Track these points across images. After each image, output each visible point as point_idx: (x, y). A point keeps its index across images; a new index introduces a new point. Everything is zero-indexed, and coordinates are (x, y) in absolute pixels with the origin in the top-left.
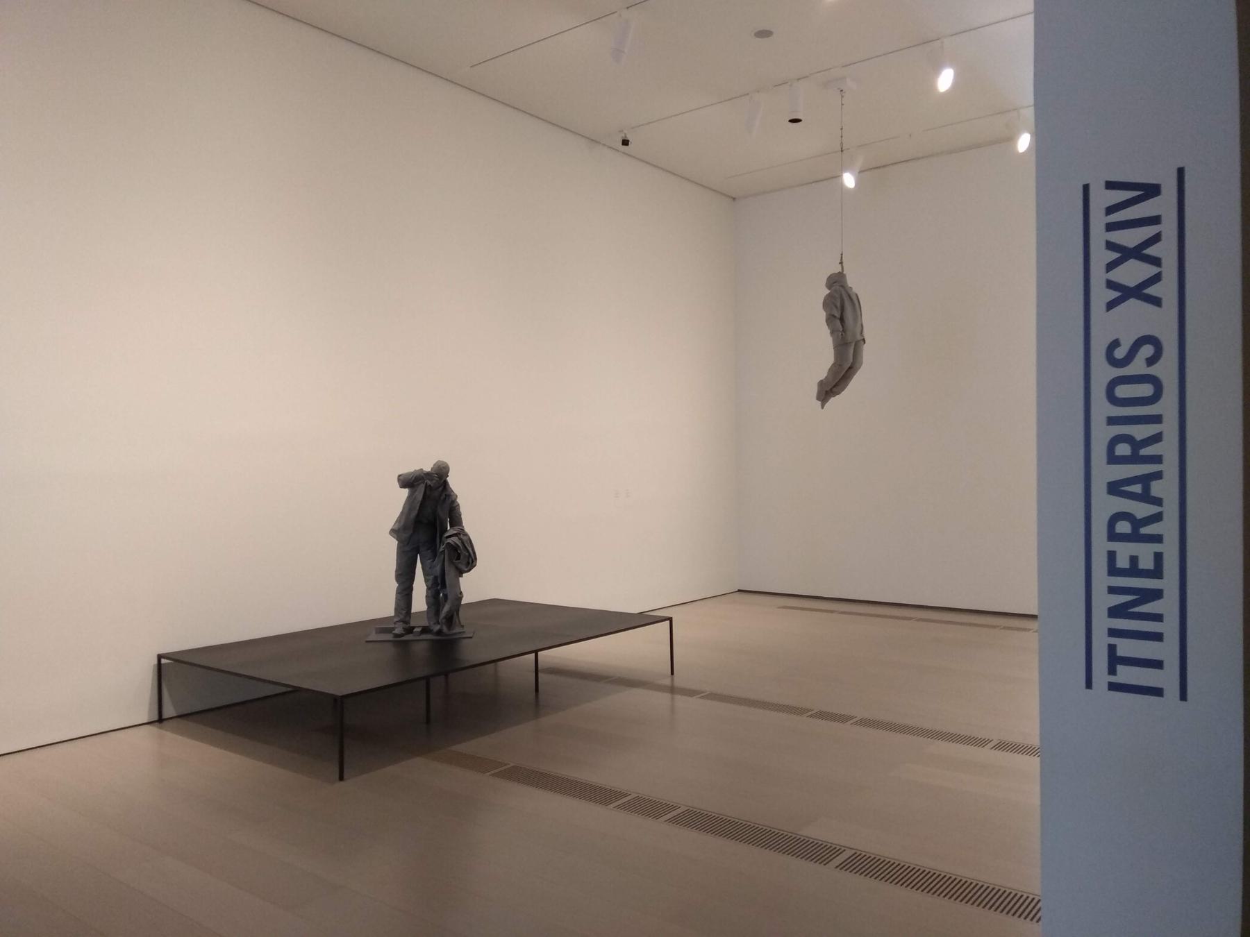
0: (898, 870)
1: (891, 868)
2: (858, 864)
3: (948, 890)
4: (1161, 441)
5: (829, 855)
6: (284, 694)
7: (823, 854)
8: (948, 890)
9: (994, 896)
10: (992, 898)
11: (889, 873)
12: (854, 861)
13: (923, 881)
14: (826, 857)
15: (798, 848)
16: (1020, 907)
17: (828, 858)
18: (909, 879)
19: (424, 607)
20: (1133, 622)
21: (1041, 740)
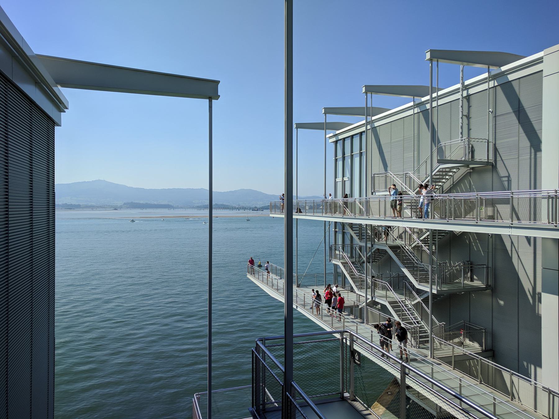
0: (27, 313)
1: (38, 307)
2: (23, 353)
3: (27, 337)
4: (543, 63)
5: (26, 349)
6: (308, 286)
7: (28, 354)
8: (27, 337)
9: (21, 322)
10: (15, 322)
11: (3, 385)
12: (39, 319)
13: (14, 354)
14: (16, 397)
15: (14, 356)
16: (13, 352)
17: (36, 353)
18: (26, 331)
19: (503, 70)
20: (394, 111)
21: (331, 133)
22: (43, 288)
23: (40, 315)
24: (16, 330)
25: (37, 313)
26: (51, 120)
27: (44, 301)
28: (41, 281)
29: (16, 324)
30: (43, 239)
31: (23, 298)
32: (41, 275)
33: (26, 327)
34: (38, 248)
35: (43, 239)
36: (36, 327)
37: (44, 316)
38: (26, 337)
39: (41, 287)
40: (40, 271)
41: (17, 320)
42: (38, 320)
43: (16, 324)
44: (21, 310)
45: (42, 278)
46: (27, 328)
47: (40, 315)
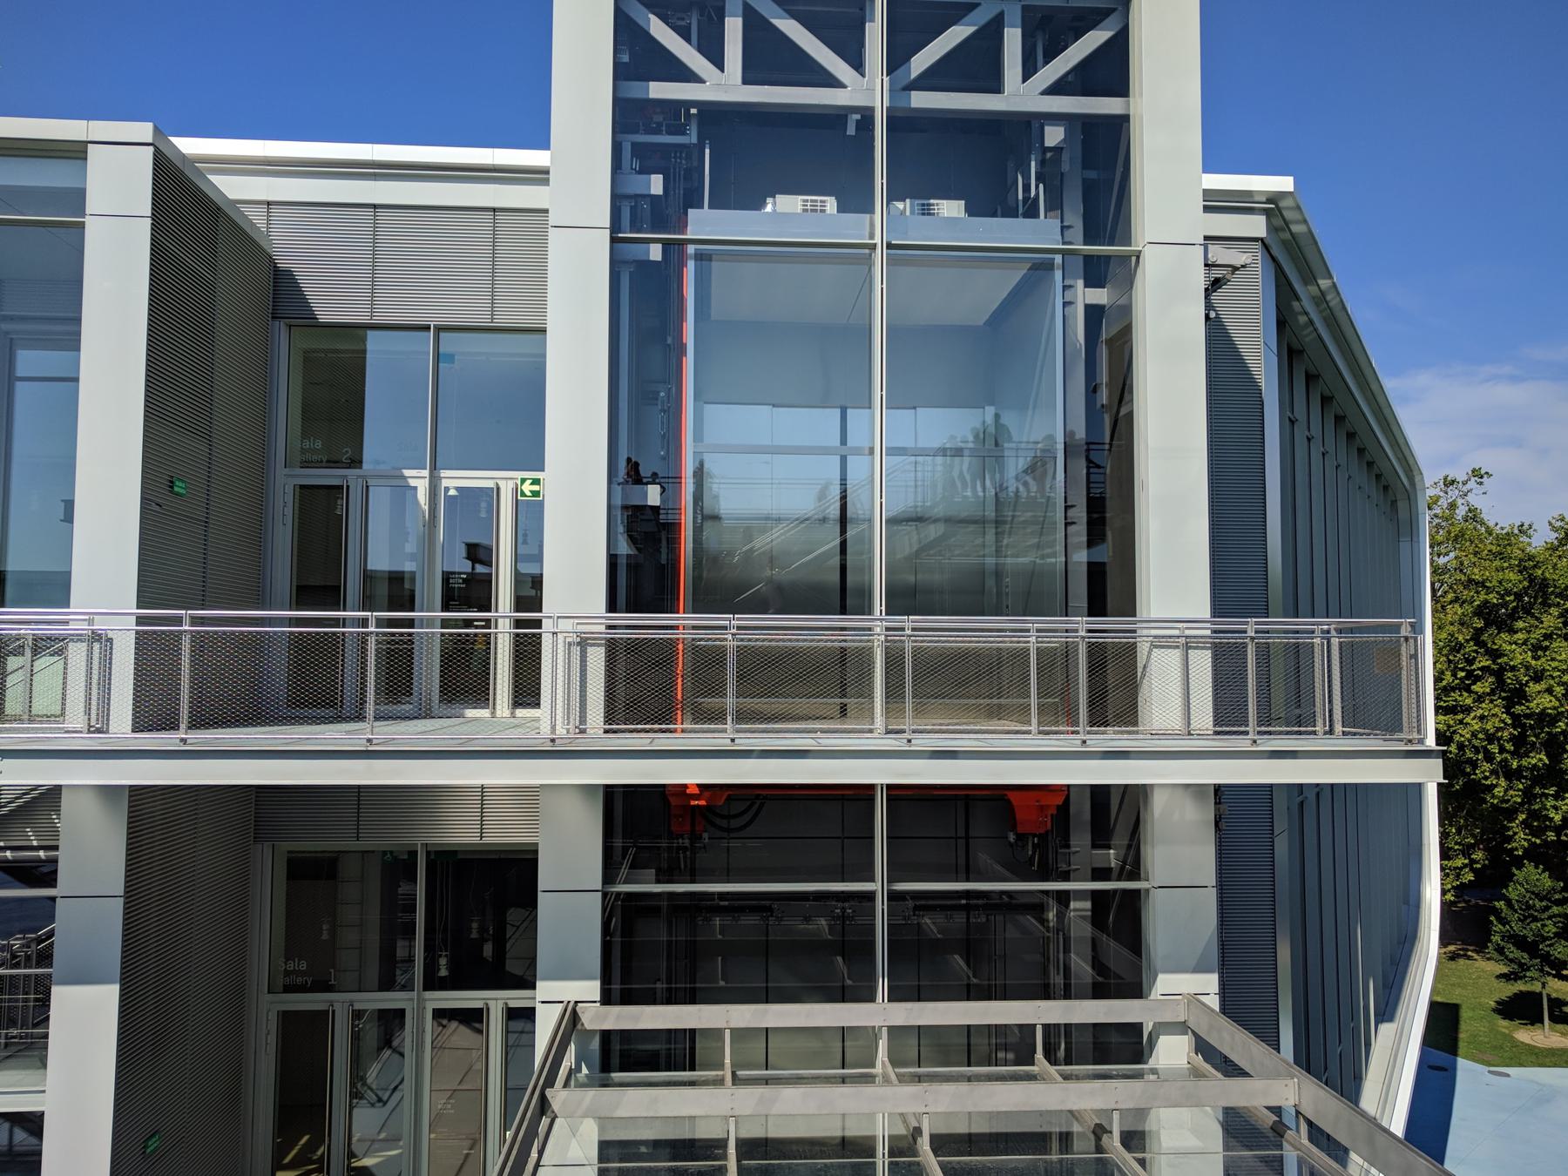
22: (178, 820)
23: (202, 416)
24: (170, 856)
25: (144, 1022)
26: (781, 1079)
27: (168, 378)
28: (144, 981)
29: (158, 304)
30: (190, 376)
31: (163, 308)
32: (162, 206)
33: (171, 873)
34: (165, 312)
35: (190, 376)
36: (139, 968)
37: (181, 912)
38: (169, 925)
39: (172, 299)
40: (163, 257)
41: (161, 321)
42: (136, 902)
43: (158, 304)
44: (162, 251)
45: (170, 923)
46: (160, 306)
47: (202, 416)
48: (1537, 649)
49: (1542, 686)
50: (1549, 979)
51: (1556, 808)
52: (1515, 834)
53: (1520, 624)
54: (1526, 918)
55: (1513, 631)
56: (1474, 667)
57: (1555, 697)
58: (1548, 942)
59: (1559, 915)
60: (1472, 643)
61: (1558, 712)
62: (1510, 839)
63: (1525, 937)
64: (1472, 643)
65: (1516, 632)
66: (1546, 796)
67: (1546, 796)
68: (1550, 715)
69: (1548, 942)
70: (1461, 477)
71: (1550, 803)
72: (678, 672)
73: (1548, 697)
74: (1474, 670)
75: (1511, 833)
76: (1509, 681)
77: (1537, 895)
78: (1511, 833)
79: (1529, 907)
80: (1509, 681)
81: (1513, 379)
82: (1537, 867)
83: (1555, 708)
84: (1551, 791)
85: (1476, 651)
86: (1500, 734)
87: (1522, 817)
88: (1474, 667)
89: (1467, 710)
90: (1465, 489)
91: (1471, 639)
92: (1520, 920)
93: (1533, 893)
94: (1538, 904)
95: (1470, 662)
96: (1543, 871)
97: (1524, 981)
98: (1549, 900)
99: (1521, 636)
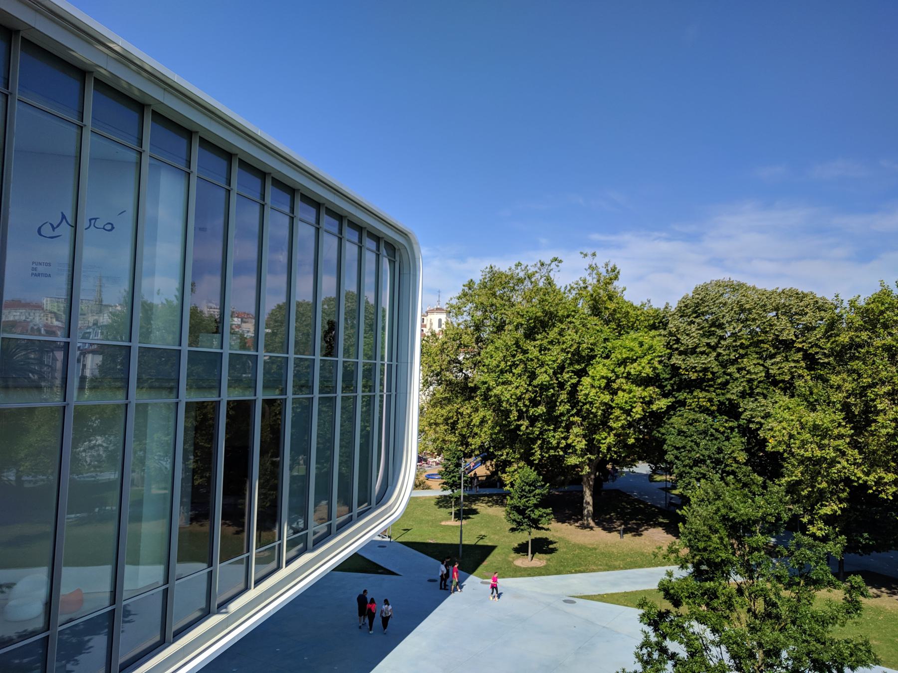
48: (542, 349)
49: (543, 370)
50: (533, 530)
51: (554, 437)
52: (536, 452)
53: (539, 336)
54: (522, 496)
55: (535, 340)
56: (515, 359)
57: (548, 375)
58: (530, 509)
59: (538, 495)
60: (514, 346)
61: (549, 384)
62: (533, 454)
63: (519, 507)
64: (514, 346)
65: (536, 340)
66: (549, 430)
67: (549, 430)
68: (546, 385)
69: (530, 509)
70: (548, 262)
71: (551, 434)
72: (872, 478)
73: (545, 375)
74: (515, 361)
75: (533, 451)
76: (529, 367)
77: (527, 484)
78: (533, 451)
79: (523, 490)
80: (529, 367)
81: (668, 240)
82: (531, 468)
83: (548, 381)
84: (552, 427)
85: (516, 351)
86: (524, 396)
87: (539, 442)
88: (515, 359)
89: (510, 383)
90: (549, 268)
91: (514, 344)
92: (519, 497)
93: (525, 482)
94: (527, 488)
95: (514, 356)
96: (534, 471)
97: (200, 523)
98: (534, 486)
99: (538, 342)
